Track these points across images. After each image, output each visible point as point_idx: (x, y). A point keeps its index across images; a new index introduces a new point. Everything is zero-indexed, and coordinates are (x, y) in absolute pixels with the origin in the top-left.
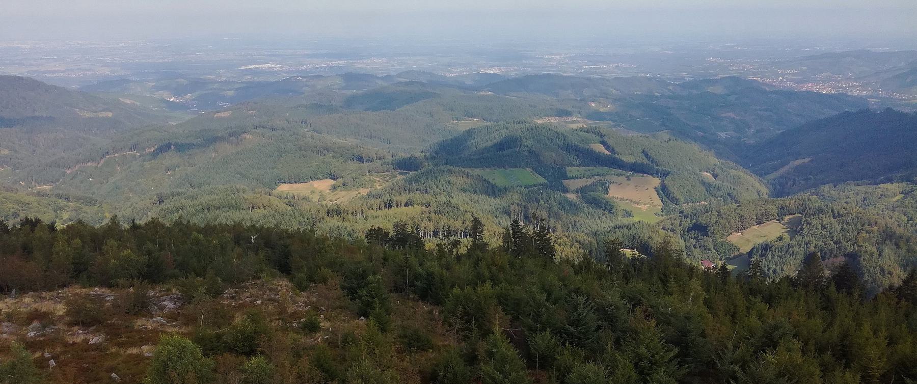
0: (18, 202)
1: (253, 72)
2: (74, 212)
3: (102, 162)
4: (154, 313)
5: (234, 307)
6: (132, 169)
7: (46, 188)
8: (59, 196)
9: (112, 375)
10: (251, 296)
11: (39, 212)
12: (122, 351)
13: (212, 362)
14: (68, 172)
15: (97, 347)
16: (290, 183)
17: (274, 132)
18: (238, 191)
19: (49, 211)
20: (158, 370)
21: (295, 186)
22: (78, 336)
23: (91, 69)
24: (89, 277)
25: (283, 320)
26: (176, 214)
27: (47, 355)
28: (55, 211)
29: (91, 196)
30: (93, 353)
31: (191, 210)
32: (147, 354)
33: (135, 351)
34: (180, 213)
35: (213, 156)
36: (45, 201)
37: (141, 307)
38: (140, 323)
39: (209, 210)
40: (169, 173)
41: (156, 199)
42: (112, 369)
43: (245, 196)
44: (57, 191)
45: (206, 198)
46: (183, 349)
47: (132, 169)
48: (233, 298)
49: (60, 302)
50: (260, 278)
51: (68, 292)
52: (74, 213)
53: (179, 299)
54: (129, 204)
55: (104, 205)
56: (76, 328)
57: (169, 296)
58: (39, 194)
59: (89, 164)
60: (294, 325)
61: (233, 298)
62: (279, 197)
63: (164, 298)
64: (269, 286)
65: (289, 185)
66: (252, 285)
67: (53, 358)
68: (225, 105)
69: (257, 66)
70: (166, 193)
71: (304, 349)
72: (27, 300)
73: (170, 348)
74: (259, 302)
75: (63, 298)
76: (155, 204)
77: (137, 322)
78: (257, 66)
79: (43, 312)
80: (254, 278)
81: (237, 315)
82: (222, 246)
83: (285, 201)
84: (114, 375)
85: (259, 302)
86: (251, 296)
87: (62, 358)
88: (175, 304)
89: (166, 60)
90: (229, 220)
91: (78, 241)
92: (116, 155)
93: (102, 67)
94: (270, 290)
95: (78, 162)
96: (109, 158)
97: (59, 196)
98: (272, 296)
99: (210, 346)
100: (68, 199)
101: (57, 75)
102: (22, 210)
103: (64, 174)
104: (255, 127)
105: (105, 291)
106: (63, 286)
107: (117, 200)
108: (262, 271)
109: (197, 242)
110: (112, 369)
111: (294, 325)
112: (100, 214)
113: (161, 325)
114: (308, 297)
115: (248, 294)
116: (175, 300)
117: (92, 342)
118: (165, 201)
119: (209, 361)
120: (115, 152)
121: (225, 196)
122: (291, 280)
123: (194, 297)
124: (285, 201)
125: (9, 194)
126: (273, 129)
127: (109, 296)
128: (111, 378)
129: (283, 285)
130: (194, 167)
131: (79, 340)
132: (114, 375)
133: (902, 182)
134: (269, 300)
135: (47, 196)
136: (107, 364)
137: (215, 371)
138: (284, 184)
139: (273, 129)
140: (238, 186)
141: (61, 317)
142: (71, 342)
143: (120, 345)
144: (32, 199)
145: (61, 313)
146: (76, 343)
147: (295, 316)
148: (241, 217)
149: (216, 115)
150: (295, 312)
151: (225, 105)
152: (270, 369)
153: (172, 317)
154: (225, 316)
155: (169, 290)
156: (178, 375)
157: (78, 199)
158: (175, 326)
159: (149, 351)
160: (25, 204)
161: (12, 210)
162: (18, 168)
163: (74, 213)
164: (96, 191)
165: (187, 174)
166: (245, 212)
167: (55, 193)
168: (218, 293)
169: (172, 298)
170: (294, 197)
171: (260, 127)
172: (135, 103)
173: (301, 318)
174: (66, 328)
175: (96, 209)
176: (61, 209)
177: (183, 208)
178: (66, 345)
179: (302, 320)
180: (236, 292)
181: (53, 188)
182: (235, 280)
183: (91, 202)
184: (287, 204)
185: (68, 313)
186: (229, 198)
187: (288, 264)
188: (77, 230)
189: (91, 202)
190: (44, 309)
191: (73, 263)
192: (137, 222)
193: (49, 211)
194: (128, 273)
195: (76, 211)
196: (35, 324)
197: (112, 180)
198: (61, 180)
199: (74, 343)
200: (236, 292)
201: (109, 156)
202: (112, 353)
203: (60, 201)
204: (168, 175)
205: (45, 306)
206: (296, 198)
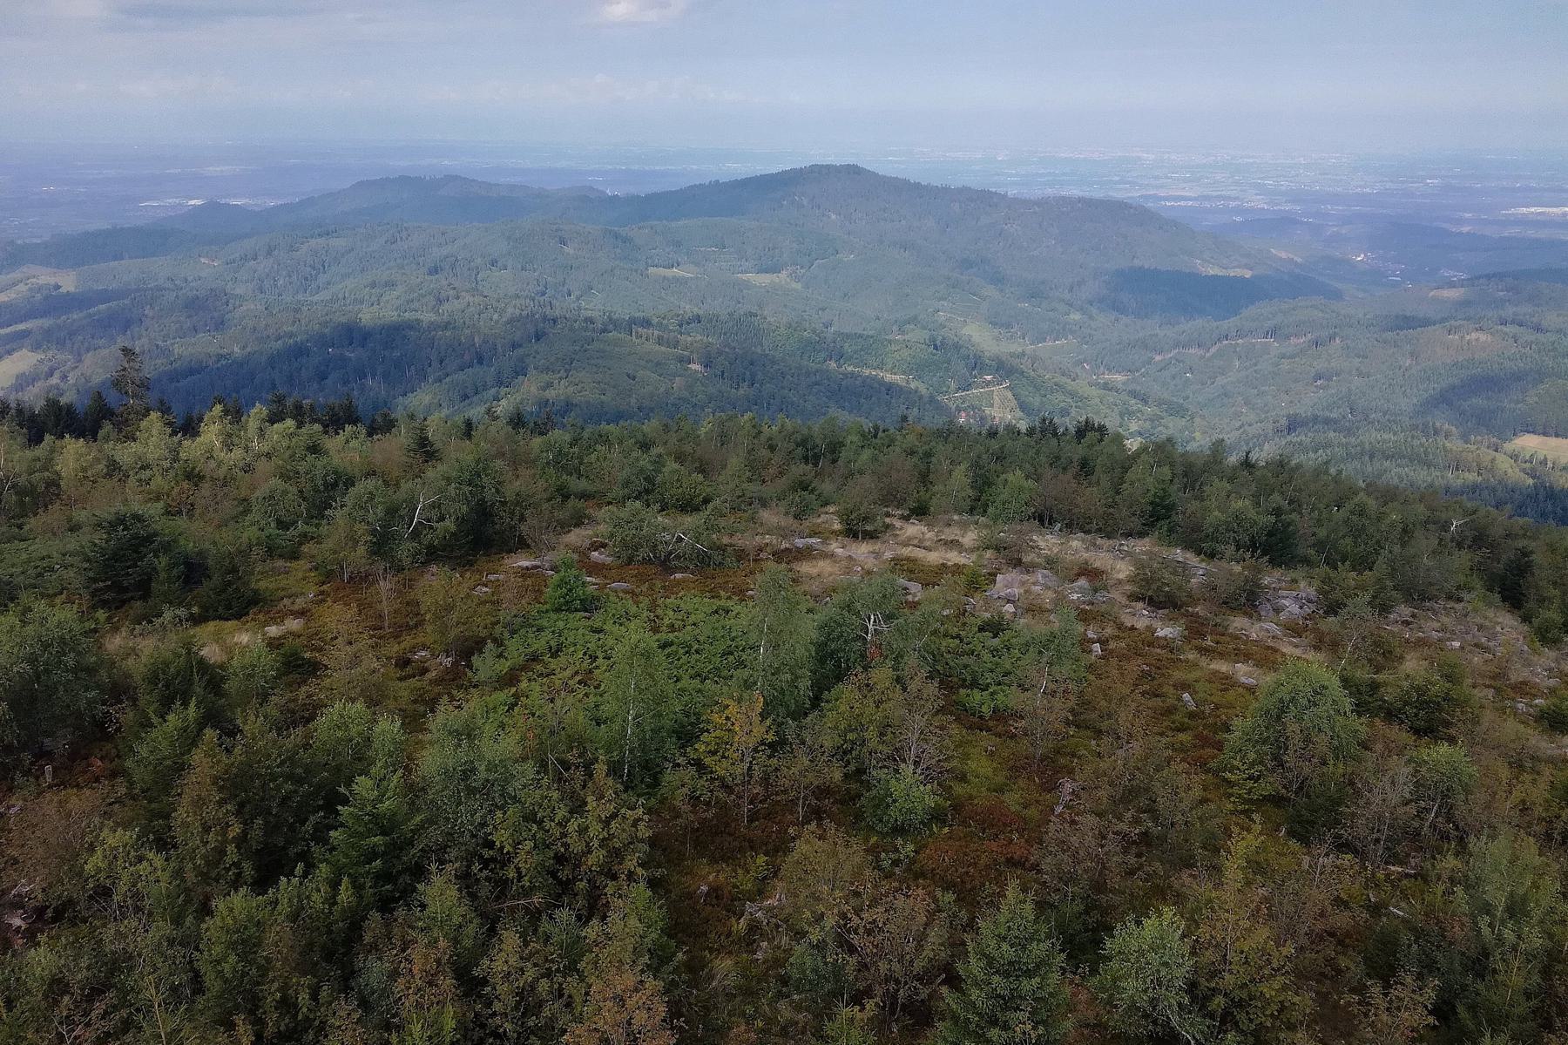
0: (1073, 395)
1: (1523, 221)
2: (1148, 423)
3: (1213, 350)
4: (1263, 613)
5: (1407, 641)
6: (1259, 367)
7: (1119, 378)
8: (1134, 394)
9: (1185, 695)
10: (1443, 629)
11: (1098, 413)
12: (1203, 662)
13: (1364, 729)
14: (1158, 358)
15: (1167, 644)
16: (1545, 434)
17: (1540, 336)
18: (1436, 432)
19: (1114, 415)
20: (1267, 712)
21: (1553, 442)
22: (1141, 618)
23: (1236, 199)
24: (1171, 530)
25: (1498, 690)
26: (1311, 455)
27: (1091, 634)
28: (1122, 415)
29: (1182, 401)
30: (1158, 651)
31: (1339, 451)
32: (1243, 680)
33: (1223, 667)
34: (1319, 454)
35: (1407, 365)
36: (1111, 397)
37: (1249, 600)
38: (1238, 623)
39: (1372, 457)
40: (1319, 383)
41: (1284, 422)
42: (1185, 686)
43: (1448, 445)
44: (1131, 387)
45: (1374, 435)
46: (1321, 690)
47: (1259, 367)
48: (1407, 623)
49: (1123, 558)
50: (1460, 600)
51: (1142, 546)
52: (1148, 425)
53: (1310, 601)
54: (1238, 425)
55: (1197, 420)
56: (1140, 605)
57: (1295, 593)
58: (1106, 387)
59: (1192, 351)
60: (1520, 706)
61: (1407, 623)
62: (1514, 457)
63: (1285, 593)
64: (1479, 620)
65: (1541, 439)
66: (1445, 609)
67: (1099, 641)
68: (1455, 276)
69: (1540, 210)
70: (1304, 415)
71: (1532, 758)
72: (1075, 544)
73: (1299, 682)
74: (1457, 644)
75: (1129, 554)
76: (1281, 431)
77: (1234, 622)
78: (1540, 210)
79: (1095, 569)
80: (1450, 597)
81: (1408, 657)
82: (1405, 531)
83: (1524, 465)
84: (1186, 696)
85: (1457, 644)
86: (1443, 629)
87: (1112, 645)
88: (1301, 608)
89: (1368, 190)
90: (1405, 482)
91: (1166, 470)
92: (1240, 341)
93: (1257, 194)
94: (1480, 628)
95: (1176, 345)
96: (1226, 344)
97: (1134, 394)
98: (1483, 640)
99: (1366, 699)
100: (1145, 401)
101: (1182, 203)
102: (1076, 407)
103: (1150, 361)
104: (1504, 323)
105: (1192, 559)
106: (1128, 535)
107: (1219, 415)
108: (1470, 590)
109: (1361, 512)
110: (1185, 686)
111: (1520, 706)
112: (1187, 432)
113: (1273, 637)
114: (1557, 661)
115: (1436, 625)
116: (1304, 601)
117: (1160, 633)
118: (1299, 430)
119: (1360, 725)
120: (1240, 337)
121: (1409, 439)
122: (1526, 619)
123: (1345, 605)
124: (1524, 465)
125: (1064, 380)
126: (1538, 329)
127: (1199, 569)
128: (1180, 699)
129: (1507, 627)
130: (1366, 379)
131: (1141, 624)
132: (1186, 696)
133: (1317, 648)
134: (1476, 645)
135: (1117, 392)
136: (1178, 675)
137: (1365, 746)
138: (1532, 435)
139: (1538, 329)
140: (1438, 424)
141: (1120, 582)
142: (1129, 625)
143: (1204, 651)
144: (1094, 392)
145: (1121, 576)
146: (1136, 629)
147: (1522, 688)
148: (1429, 479)
149: (1432, 293)
150: (1524, 683)
151: (1455, 276)
152: (1471, 776)
153: (1294, 630)
154: (1390, 652)
155: (1294, 581)
156: (1301, 731)
157: (1160, 403)
158: (1296, 646)
159: (1247, 675)
160: (1082, 398)
161: (1062, 405)
162: (1087, 343)
163: (1148, 425)
164: (1191, 395)
165: (1350, 390)
166: (1438, 474)
167: (1129, 388)
168: (1385, 609)
169: (1300, 596)
170: (1544, 462)
171: (1513, 322)
172: (1295, 259)
173: (1535, 696)
174: (1124, 601)
175: (1183, 424)
176: (1131, 414)
177: (1328, 445)
178: (1120, 626)
179: (1537, 701)
180: (1414, 616)
181: (1128, 379)
182: (1418, 594)
183: (1178, 411)
184: (1528, 474)
185: (1131, 580)
186: (1416, 442)
187: (1520, 586)
188: (1162, 451)
189: (1178, 411)
190: (1097, 564)
191: (1152, 503)
192: (1254, 457)
193: (1114, 415)
194: (1234, 537)
195: (1152, 421)
196: (1082, 582)
197: (1220, 380)
198: (1143, 370)
199: (1133, 628)
200: (1414, 616)
201: (1227, 342)
202: (1187, 661)
203: (1133, 402)
204: (1316, 386)
205: (1101, 558)
206: (1550, 465)
